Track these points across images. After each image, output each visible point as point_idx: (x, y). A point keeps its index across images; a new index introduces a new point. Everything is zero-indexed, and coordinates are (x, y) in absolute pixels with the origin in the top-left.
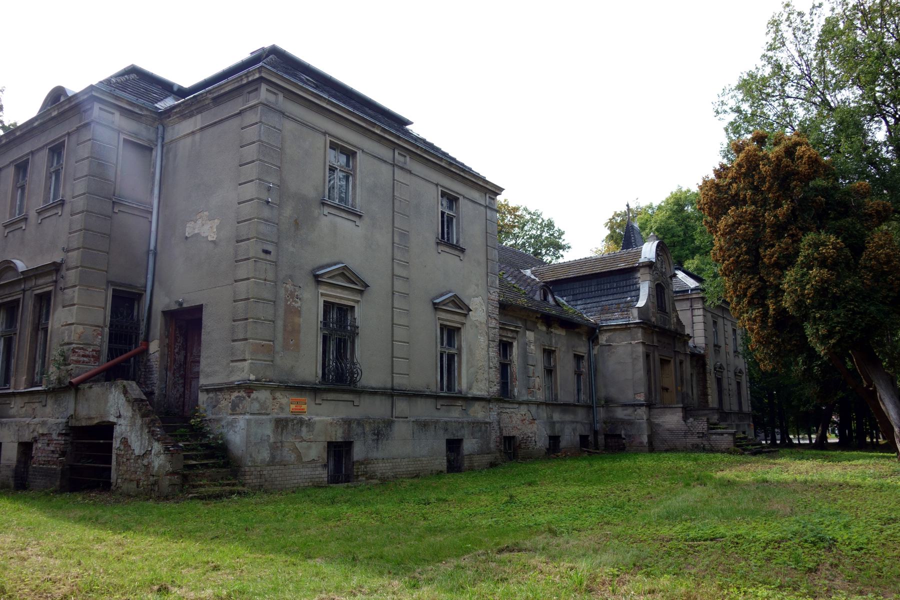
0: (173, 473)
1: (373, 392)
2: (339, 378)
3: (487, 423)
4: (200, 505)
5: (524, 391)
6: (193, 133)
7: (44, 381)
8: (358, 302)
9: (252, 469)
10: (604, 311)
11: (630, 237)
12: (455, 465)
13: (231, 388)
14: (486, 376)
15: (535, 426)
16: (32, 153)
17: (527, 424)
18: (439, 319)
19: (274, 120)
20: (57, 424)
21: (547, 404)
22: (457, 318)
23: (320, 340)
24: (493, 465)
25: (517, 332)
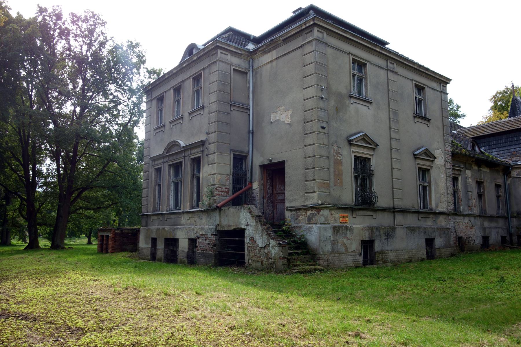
0: (284, 258)
1: (383, 210)
2: (365, 203)
3: (448, 228)
4: (300, 276)
5: (466, 208)
6: (271, 61)
7: (200, 205)
8: (372, 155)
9: (323, 256)
10: (513, 155)
11: (515, 107)
12: (431, 255)
13: (306, 209)
14: (446, 199)
15: (474, 230)
16: (183, 81)
17: (471, 230)
18: (418, 164)
19: (322, 48)
20: (211, 229)
21: (480, 216)
22: (428, 163)
23: (353, 179)
24: (452, 255)
25: (461, 171)
